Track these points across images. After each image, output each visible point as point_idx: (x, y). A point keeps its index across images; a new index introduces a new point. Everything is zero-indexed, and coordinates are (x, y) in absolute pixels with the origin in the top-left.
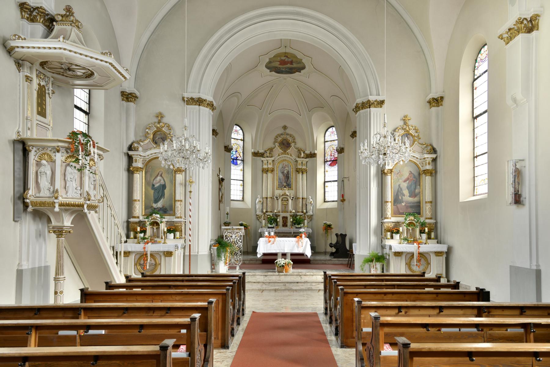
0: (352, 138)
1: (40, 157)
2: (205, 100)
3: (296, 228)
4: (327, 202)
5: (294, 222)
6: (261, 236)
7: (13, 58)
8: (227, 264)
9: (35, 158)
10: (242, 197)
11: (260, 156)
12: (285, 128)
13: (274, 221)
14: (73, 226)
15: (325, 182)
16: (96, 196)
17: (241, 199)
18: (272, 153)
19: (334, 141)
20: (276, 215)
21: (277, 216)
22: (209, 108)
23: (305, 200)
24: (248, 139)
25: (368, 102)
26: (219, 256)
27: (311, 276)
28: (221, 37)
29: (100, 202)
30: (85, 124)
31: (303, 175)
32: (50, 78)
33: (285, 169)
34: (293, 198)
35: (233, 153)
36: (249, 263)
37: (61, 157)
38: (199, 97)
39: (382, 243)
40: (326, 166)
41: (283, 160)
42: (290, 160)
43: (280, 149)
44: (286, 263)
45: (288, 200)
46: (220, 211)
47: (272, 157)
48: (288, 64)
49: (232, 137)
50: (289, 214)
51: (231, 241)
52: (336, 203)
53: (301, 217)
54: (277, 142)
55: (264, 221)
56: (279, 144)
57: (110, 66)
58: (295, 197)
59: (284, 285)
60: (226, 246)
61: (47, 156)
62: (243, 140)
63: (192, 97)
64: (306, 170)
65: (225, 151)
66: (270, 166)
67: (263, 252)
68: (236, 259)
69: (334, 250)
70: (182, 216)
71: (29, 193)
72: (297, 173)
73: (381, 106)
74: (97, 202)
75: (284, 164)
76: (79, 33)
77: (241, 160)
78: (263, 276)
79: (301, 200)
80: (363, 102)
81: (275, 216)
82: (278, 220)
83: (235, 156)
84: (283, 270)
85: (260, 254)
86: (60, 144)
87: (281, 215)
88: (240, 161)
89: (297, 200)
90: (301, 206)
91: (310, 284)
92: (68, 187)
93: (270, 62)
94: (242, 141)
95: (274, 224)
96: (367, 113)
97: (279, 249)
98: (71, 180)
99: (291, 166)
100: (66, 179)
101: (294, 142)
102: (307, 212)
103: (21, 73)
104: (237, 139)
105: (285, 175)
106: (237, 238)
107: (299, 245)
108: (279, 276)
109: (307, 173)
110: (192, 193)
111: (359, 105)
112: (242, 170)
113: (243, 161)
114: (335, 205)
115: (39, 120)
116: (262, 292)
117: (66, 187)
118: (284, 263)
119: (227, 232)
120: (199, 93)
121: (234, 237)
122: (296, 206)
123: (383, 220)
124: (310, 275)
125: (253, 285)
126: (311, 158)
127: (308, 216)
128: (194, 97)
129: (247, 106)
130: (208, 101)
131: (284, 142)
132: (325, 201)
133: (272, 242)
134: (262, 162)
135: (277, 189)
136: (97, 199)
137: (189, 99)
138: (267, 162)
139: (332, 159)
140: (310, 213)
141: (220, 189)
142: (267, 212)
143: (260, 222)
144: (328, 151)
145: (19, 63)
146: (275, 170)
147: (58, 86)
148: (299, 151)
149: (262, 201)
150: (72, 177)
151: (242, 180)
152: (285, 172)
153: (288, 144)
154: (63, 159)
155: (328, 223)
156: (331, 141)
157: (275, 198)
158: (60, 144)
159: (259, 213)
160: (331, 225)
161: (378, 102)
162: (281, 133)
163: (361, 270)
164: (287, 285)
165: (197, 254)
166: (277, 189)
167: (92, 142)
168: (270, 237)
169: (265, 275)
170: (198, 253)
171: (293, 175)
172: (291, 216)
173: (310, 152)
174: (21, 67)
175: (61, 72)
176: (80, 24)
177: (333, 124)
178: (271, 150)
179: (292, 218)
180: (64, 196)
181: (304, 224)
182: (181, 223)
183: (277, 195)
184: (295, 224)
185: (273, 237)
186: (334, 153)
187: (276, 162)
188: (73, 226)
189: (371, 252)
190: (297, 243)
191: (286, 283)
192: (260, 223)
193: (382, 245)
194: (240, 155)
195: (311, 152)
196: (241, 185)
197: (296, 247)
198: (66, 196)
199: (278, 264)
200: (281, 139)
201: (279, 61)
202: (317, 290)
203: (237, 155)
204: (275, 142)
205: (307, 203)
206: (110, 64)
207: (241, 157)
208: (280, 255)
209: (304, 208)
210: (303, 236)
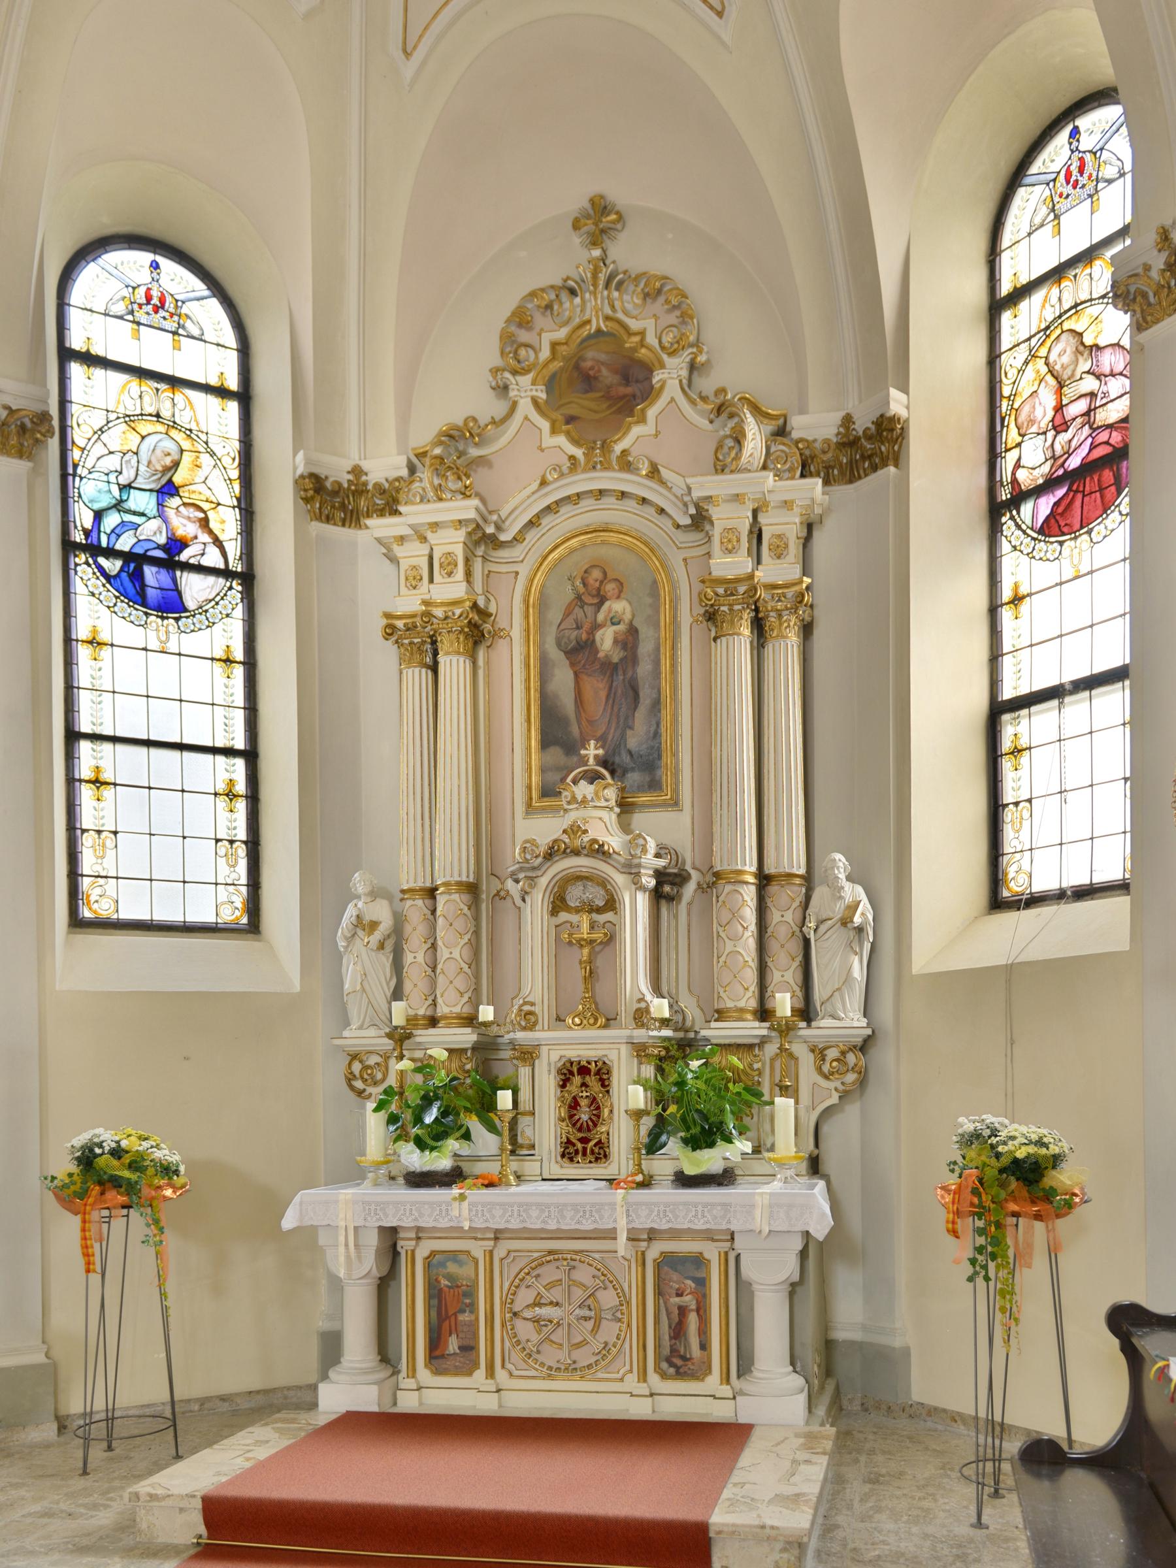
17: (233, 911)
33: (601, 617)
35: (131, 504)
43: (554, 431)
45: (611, 904)
52: (1121, 903)
54: (525, 371)
56: (551, 384)
77: (225, 573)
79: (749, 894)
83: (153, 532)
88: (211, 579)
94: (233, 407)
102: (806, 1013)
104: (174, 382)
109: (818, 633)
112: (239, 655)
131: (592, 355)
132: (997, 903)
139: (1068, 453)
144: (1026, 385)
151: (240, 744)
152: (606, 639)
153: (627, 379)
160: (1056, 1160)
172: (640, 1051)
173: (837, 417)
186: (1090, 384)
195: (848, 420)
196: (231, 795)
200: (562, 334)
207: (218, 543)
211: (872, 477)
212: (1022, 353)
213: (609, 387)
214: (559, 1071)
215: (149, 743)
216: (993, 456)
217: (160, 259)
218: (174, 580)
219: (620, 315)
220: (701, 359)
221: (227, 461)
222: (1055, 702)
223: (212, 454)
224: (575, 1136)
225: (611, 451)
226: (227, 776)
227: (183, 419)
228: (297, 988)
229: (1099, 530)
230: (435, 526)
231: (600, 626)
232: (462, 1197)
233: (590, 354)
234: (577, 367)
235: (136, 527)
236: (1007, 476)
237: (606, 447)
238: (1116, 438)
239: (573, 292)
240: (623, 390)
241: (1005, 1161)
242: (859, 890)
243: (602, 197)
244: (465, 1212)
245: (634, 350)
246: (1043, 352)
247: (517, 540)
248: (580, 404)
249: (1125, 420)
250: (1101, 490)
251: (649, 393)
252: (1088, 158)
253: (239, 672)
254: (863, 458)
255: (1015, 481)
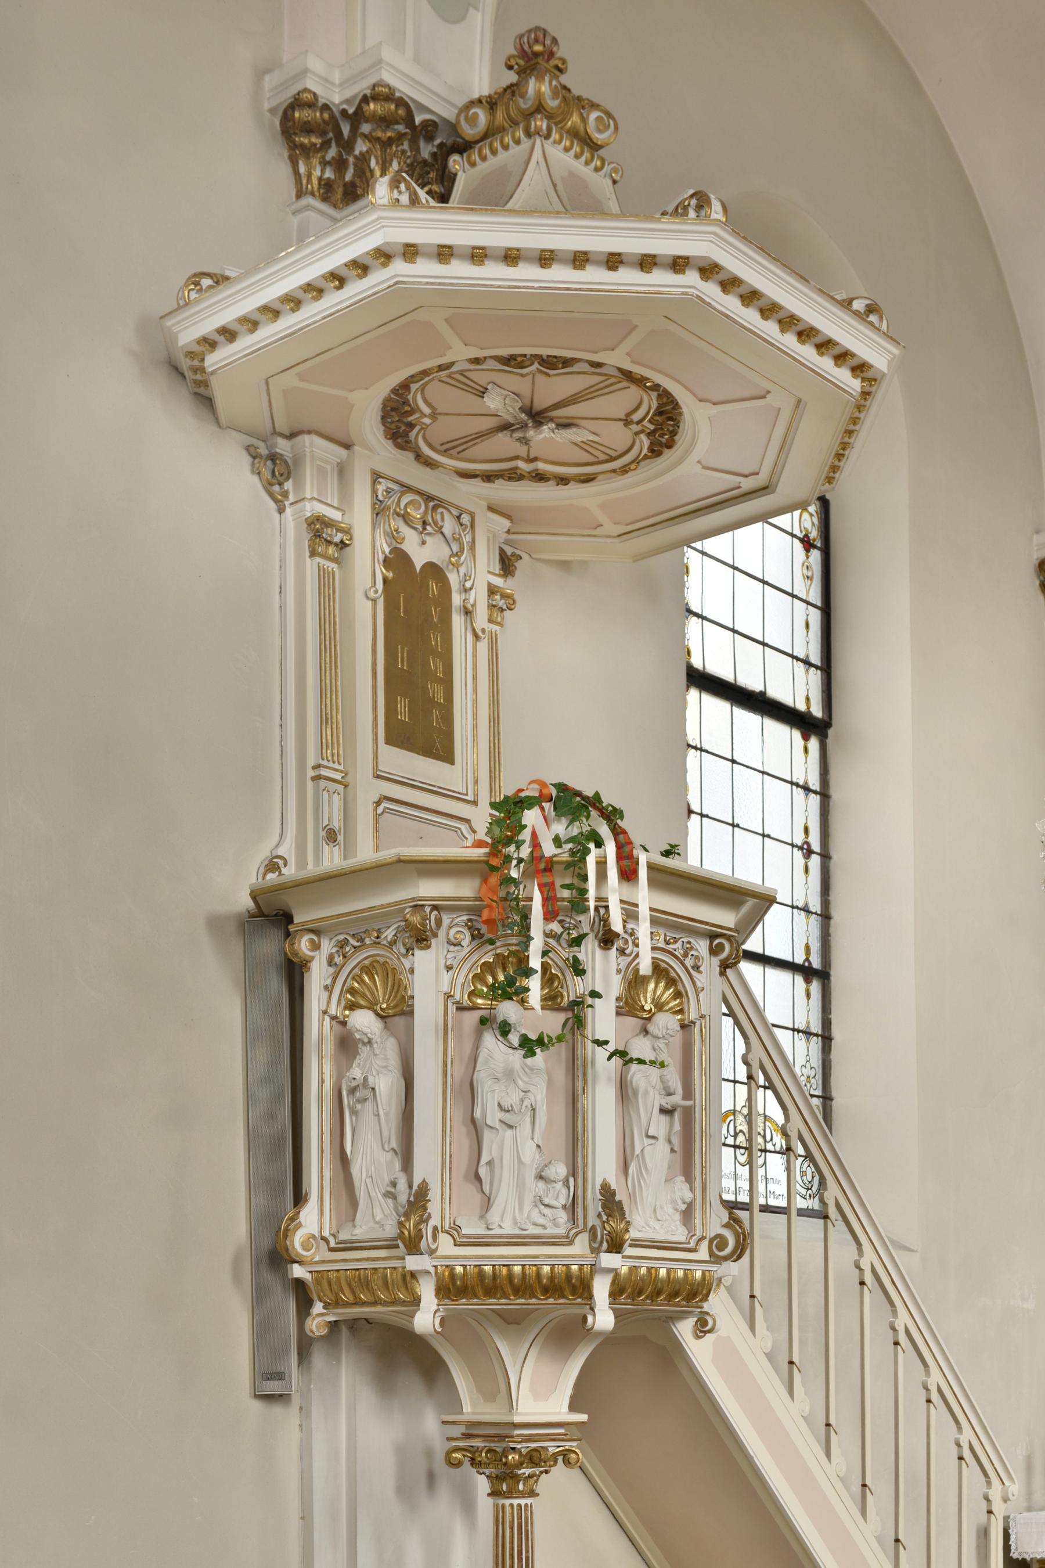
1: (352, 991)
7: (234, 434)
9: (329, 1003)
14: (583, 1417)
16: (698, 1214)
29: (726, 1258)
30: (801, 791)
32: (472, 515)
37: (446, 977)
57: (711, 290)
61: (385, 984)
71: (300, 1225)
74: (703, 1254)
76: (595, 175)
86: (430, 889)
92: (490, 1163)
98: (507, 1117)
100: (478, 1114)
103: (289, 511)
115: (399, 773)
117: (483, 1171)
136: (703, 1238)
145: (273, 458)
147: (565, 565)
150: (512, 1099)
154: (460, 984)
158: (430, 889)
167: (610, 849)
174: (287, 479)
175: (517, 458)
176: (594, 115)
180: (471, 1228)
188: (583, 1417)
198: (481, 1231)
206: (709, 270)
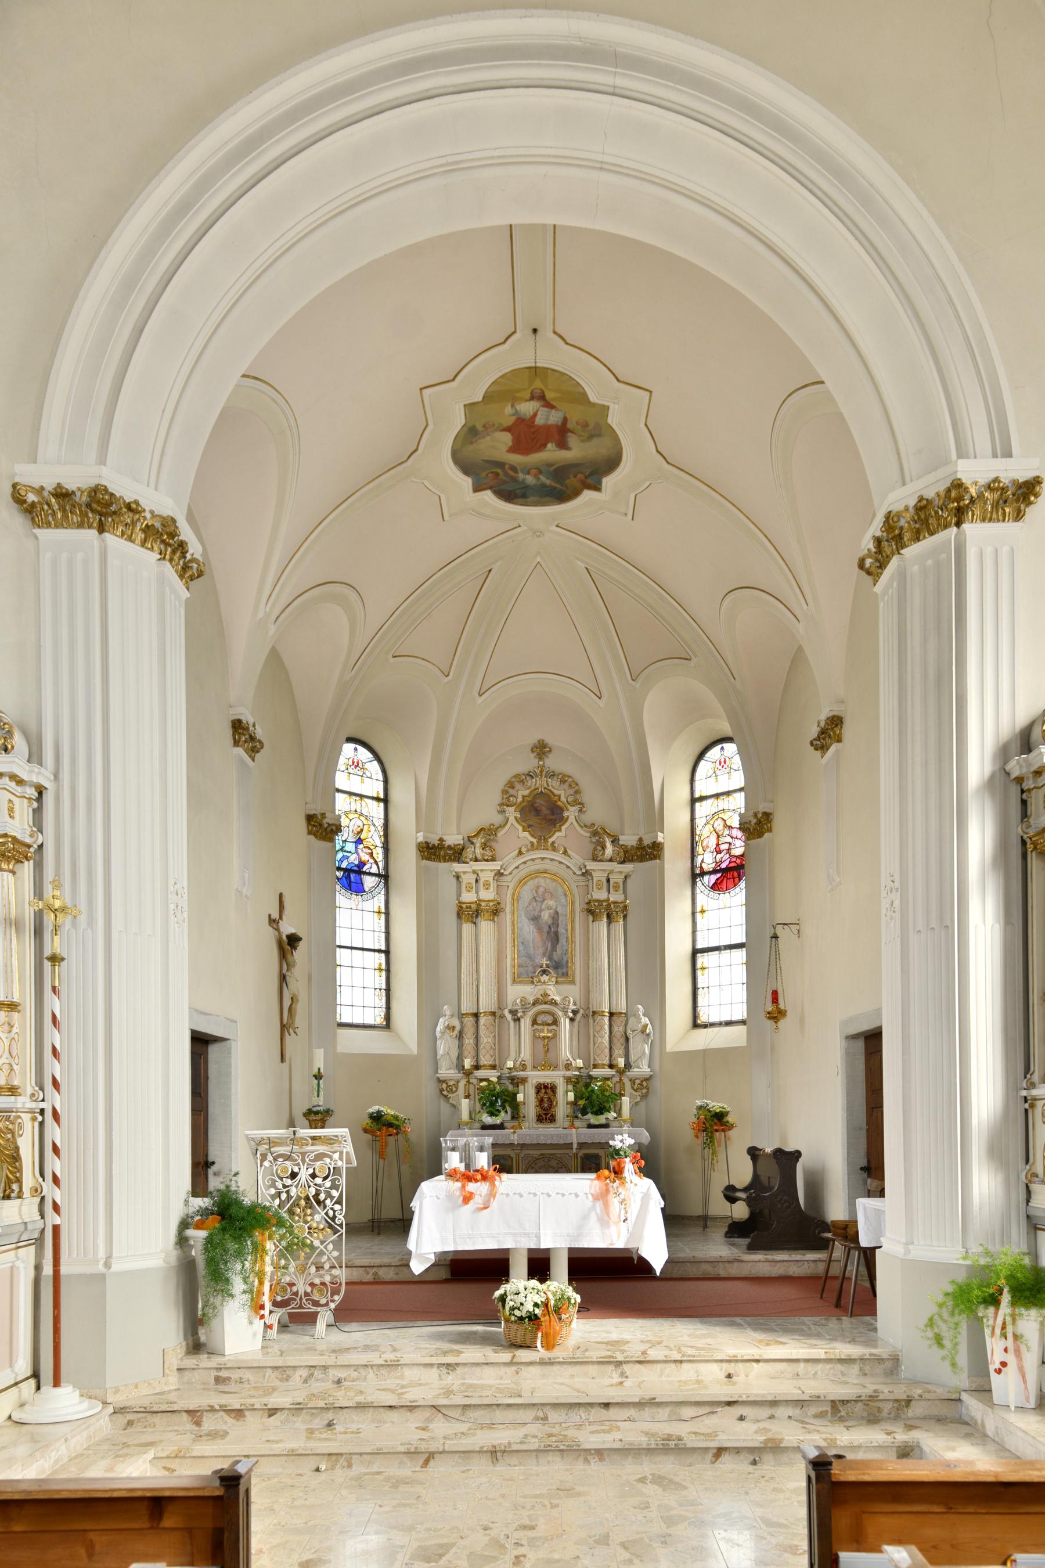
0: (819, 753)
2: (129, 507)
3: (590, 1126)
4: (705, 1026)
5: (581, 1103)
6: (435, 1169)
8: (262, 1312)
10: (382, 1013)
11: (450, 860)
12: (541, 749)
13: (504, 1102)
15: (695, 952)
17: (380, 1020)
18: (493, 844)
19: (728, 793)
20: (512, 1079)
21: (518, 1082)
22: (156, 548)
23: (623, 1019)
24: (403, 796)
25: (953, 494)
26: (219, 1278)
27: (673, 1366)
28: (205, 184)
31: (612, 925)
33: (543, 907)
34: (575, 1012)
35: (346, 849)
36: (396, 1278)
38: (97, 486)
39: (1028, 1201)
40: (698, 891)
41: (538, 872)
42: (561, 870)
43: (524, 831)
44: (546, 1305)
45: (555, 1022)
46: (286, 1065)
47: (493, 859)
48: (549, 445)
49: (338, 785)
50: (563, 1073)
51: (289, 1197)
52: (743, 1029)
53: (609, 1083)
54: (512, 806)
55: (465, 1104)
58: (581, 1011)
59: (537, 1418)
60: (254, 1227)
62: (386, 801)
63: (59, 485)
64: (625, 907)
65: (310, 833)
66: (487, 895)
67: (440, 1249)
68: (317, 1281)
69: (740, 1211)
70: (16, 1083)
72: (591, 918)
73: (1019, 511)
75: (538, 887)
77: (378, 875)
78: (434, 1372)
79: (606, 1020)
80: (921, 499)
81: (507, 1083)
82: (520, 1097)
83: (354, 859)
84: (535, 1338)
85: (422, 1257)
87: (530, 1080)
88: (374, 878)
89: (591, 1021)
90: (607, 1045)
91: (667, 1410)
93: (470, 433)
94: (382, 805)
95: (503, 1114)
96: (944, 556)
97: (514, 1235)
99: (565, 895)
101: (576, 802)
102: (628, 1066)
104: (361, 796)
105: (546, 929)
106: (318, 1181)
107: (611, 1209)
108: (514, 1368)
109: (629, 918)
110: (64, 964)
111: (902, 522)
112: (383, 910)
113: (385, 877)
114: (736, 1036)
116: (426, 1462)
118: (536, 1305)
119: (270, 1157)
120: (102, 460)
121: (303, 1180)
122: (589, 1042)
123: (1032, 1085)
124: (665, 1362)
125: (385, 1422)
126: (641, 861)
127: (633, 1081)
128: (70, 485)
129: (392, 660)
130: (148, 515)
131: (539, 802)
132: (695, 1025)
133: (477, 1201)
134: (455, 880)
135: (514, 982)
137: (46, 494)
138: (477, 881)
140: (642, 1069)
141: (283, 978)
142: (477, 1067)
143: (454, 1106)
144: (705, 833)
146: (508, 910)
148: (598, 834)
149: (458, 1028)
151: (383, 948)
152: (546, 916)
155: (716, 1106)
156: (717, 796)
157: (509, 1017)
159: (447, 1071)
160: (727, 1113)
161: (1003, 490)
162: (526, 771)
163: (930, 1346)
164: (553, 1416)
165: (101, 1268)
166: (514, 982)
168: (469, 1176)
169: (448, 1365)
170: (107, 1265)
171: (575, 926)
172: (568, 1080)
173: (637, 838)
177: (727, 729)
178: (489, 833)
179: (575, 1091)
181: (619, 1113)
182: (8, 1119)
183: (514, 1003)
184: (584, 1113)
185: (484, 1178)
186: (728, 839)
187: (510, 882)
189: (975, 1249)
190: (599, 1205)
191: (547, 1409)
192: (453, 1109)
193: (1031, 1212)
194: (375, 855)
195: (641, 840)
196: (380, 970)
197: (593, 1222)
199: (507, 1308)
200: (526, 792)
201: (508, 429)
202: (707, 1449)
203: (362, 855)
204: (505, 804)
205: (629, 1032)
207: (376, 863)
208: (519, 1267)
209: (618, 1050)
210: (629, 1167)
211: (650, 862)
212: (704, 821)
213: (546, 815)
214: (536, 1087)
215: (352, 948)
216: (693, 855)
217: (358, 747)
218: (361, 879)
219: (550, 788)
220: (584, 809)
221: (379, 828)
222: (717, 952)
223: (374, 825)
224: (542, 1112)
225: (548, 842)
226: (379, 961)
227: (364, 812)
228: (415, 1052)
229: (733, 892)
230: (482, 871)
231: (544, 910)
232: (514, 1132)
233: (538, 801)
234: (532, 805)
235: (348, 857)
236: (698, 864)
237: (546, 840)
238: (738, 861)
239: (532, 777)
240: (552, 817)
241: (713, 1113)
242: (647, 1019)
243: (543, 741)
244: (516, 1138)
245: (556, 801)
246: (712, 822)
247: (510, 873)
248: (533, 820)
249: (742, 855)
250: (734, 878)
251: (563, 820)
252: (727, 759)
253: (383, 916)
254: (646, 854)
255: (701, 867)
